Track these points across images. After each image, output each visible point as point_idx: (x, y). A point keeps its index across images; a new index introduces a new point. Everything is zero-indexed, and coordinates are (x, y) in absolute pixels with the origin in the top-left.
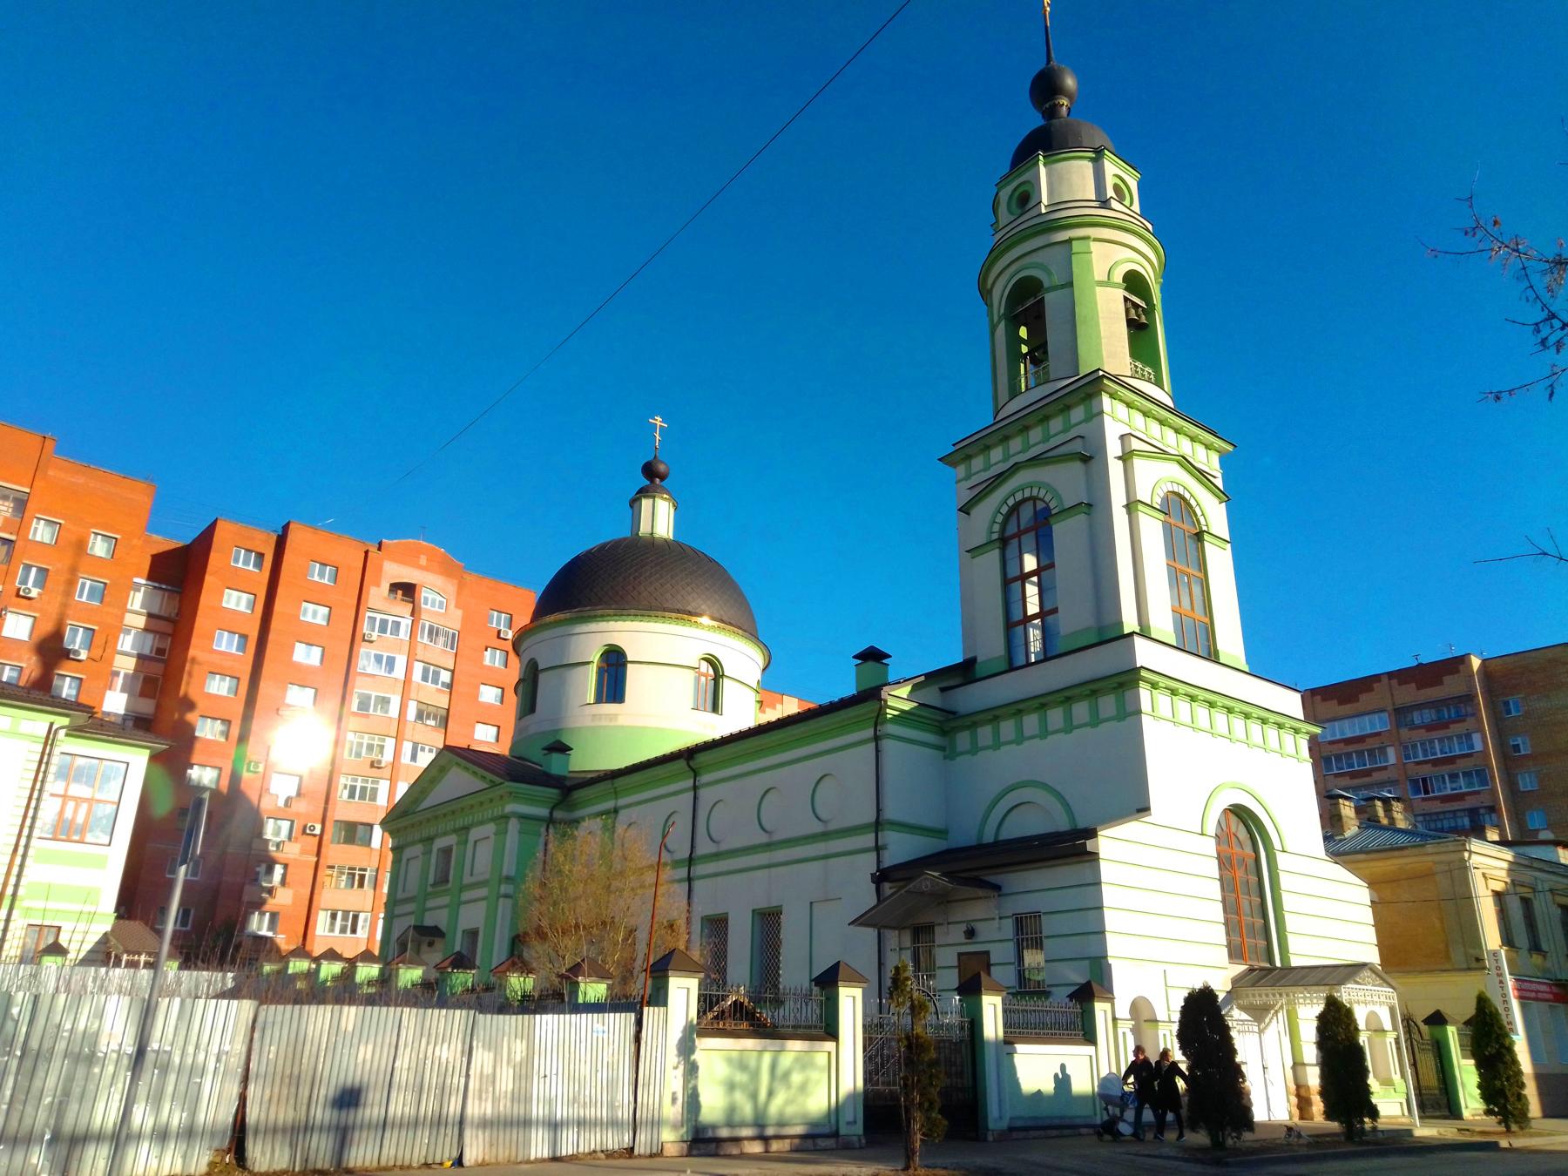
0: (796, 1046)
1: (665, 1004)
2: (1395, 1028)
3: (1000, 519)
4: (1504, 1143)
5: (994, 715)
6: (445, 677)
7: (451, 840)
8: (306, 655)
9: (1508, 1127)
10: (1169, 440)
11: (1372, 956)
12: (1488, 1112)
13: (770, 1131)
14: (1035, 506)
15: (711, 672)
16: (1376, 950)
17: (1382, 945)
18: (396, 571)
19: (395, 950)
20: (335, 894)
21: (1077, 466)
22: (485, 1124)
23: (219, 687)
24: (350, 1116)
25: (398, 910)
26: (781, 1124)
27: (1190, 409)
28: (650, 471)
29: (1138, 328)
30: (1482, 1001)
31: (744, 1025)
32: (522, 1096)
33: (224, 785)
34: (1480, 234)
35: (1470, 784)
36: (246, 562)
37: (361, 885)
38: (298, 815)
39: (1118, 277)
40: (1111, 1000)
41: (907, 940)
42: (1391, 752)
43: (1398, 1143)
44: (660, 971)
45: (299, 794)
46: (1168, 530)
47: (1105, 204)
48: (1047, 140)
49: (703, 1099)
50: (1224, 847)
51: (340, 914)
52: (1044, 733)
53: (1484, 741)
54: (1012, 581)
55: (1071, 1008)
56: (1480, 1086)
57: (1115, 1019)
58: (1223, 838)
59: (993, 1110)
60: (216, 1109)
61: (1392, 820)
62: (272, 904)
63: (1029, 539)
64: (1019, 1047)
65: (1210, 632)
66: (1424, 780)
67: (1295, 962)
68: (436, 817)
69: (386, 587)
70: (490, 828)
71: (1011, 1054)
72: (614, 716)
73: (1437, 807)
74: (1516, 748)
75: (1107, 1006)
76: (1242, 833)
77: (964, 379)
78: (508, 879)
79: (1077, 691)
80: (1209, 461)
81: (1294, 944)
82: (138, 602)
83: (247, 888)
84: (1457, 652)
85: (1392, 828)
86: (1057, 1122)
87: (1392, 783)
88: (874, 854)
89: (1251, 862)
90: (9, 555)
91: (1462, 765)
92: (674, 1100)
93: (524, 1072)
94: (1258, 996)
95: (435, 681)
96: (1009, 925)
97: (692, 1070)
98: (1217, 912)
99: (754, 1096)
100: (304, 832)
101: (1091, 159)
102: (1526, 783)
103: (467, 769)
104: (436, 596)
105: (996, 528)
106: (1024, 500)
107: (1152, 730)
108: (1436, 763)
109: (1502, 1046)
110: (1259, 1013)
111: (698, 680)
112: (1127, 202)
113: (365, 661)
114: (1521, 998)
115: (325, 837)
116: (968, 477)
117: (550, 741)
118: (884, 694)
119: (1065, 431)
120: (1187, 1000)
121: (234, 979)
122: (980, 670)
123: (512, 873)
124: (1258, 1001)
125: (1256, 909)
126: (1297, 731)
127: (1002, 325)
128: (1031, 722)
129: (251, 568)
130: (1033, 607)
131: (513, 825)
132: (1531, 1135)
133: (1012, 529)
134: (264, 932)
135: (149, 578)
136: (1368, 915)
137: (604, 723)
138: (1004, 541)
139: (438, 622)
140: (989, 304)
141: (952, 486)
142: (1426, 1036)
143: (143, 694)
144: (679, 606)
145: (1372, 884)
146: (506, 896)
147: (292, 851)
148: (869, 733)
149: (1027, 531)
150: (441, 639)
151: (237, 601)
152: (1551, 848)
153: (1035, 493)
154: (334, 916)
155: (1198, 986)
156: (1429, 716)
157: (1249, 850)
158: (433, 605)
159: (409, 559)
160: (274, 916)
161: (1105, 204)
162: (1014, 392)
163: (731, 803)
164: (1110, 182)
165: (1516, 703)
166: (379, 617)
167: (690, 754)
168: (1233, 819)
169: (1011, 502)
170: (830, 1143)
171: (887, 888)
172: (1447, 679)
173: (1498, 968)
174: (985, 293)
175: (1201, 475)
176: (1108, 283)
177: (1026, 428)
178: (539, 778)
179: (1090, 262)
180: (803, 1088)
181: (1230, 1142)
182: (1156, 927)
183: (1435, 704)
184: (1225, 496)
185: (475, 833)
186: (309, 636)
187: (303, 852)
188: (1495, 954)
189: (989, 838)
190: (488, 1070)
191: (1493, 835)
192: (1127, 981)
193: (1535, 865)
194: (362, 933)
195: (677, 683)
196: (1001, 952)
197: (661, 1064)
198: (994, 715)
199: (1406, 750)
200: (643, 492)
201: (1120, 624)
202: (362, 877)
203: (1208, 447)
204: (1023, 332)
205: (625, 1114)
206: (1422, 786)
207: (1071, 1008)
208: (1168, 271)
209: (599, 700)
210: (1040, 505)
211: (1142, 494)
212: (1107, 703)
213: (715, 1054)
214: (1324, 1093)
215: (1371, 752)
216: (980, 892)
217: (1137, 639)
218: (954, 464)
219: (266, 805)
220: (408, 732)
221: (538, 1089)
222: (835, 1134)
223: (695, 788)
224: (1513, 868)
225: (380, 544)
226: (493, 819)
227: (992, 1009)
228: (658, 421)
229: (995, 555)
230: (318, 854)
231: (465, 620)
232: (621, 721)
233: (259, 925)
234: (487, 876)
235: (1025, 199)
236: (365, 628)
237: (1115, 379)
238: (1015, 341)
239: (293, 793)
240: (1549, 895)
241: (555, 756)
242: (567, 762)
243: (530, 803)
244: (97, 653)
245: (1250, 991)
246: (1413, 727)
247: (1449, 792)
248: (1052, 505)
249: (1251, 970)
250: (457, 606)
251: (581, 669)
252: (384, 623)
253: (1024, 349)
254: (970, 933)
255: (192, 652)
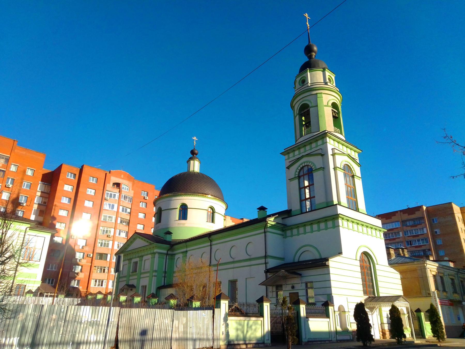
0: (253, 319)
1: (220, 307)
2: (408, 313)
3: (298, 171)
4: (439, 345)
5: (297, 226)
6: (129, 210)
7: (137, 259)
8: (88, 204)
9: (439, 341)
10: (345, 150)
11: (401, 293)
12: (434, 336)
13: (247, 342)
14: (308, 167)
15: (212, 211)
16: (402, 292)
17: (404, 290)
18: (114, 179)
19: (120, 291)
20: (96, 275)
21: (320, 157)
22: (177, 340)
23: (63, 213)
24: (144, 337)
25: (121, 280)
26: (250, 340)
27: (350, 140)
28: (193, 152)
29: (336, 118)
30: (432, 306)
31: (238, 313)
32: (185, 332)
33: (64, 242)
34: (447, 138)
35: (423, 243)
36: (71, 177)
37: (104, 272)
38: (86, 251)
39: (330, 104)
40: (333, 306)
41: (274, 289)
42: (401, 233)
43: (411, 344)
44: (218, 298)
45: (86, 245)
46: (345, 175)
47: (326, 84)
48: (309, 65)
49: (230, 333)
50: (362, 263)
51: (98, 281)
52: (312, 231)
53: (427, 230)
54: (302, 188)
55: (323, 308)
56: (431, 329)
57: (334, 311)
58: (361, 261)
59: (303, 337)
60: (111, 336)
61: (404, 254)
62: (78, 277)
63: (306, 177)
64: (310, 319)
65: (356, 203)
66: (410, 241)
67: (381, 295)
68: (130, 254)
69: (111, 184)
70: (150, 256)
71: (308, 321)
72: (184, 224)
73: (414, 249)
74: (436, 232)
75: (332, 307)
76: (366, 259)
77: (286, 132)
78: (156, 271)
79: (321, 220)
80: (355, 155)
81: (381, 290)
82: (39, 187)
83: (71, 273)
84: (419, 205)
85: (404, 256)
86: (320, 340)
87: (402, 242)
88: (265, 265)
89: (368, 267)
90: (4, 175)
91: (421, 237)
92: (223, 334)
93: (186, 326)
94: (371, 304)
95: (126, 212)
96: (304, 285)
97: (227, 325)
98: (360, 281)
99: (243, 332)
100: (87, 256)
101: (322, 71)
102: (439, 242)
103: (142, 239)
104: (126, 187)
105: (297, 173)
106: (305, 166)
107: (342, 231)
108: (414, 236)
109: (437, 318)
110: (372, 309)
111: (208, 213)
112: (332, 83)
113: (106, 206)
114: (441, 305)
115: (94, 258)
116: (289, 158)
117: (165, 231)
118: (267, 220)
119: (316, 147)
120: (356, 306)
121: (80, 300)
122: (293, 213)
123: (157, 269)
124: (372, 306)
125: (370, 281)
126: (380, 231)
127: (298, 116)
128: (308, 228)
129: (72, 178)
130: (308, 196)
131: (157, 255)
132: (445, 342)
133: (301, 174)
134: (75, 286)
135: (41, 181)
136: (400, 282)
137: (181, 226)
138: (299, 177)
139: (127, 194)
140: (294, 111)
141: (283, 161)
142: (416, 315)
143: (40, 215)
144: (203, 192)
145: (401, 272)
146: (155, 276)
147: (84, 262)
148: (263, 231)
149: (306, 174)
150: (128, 199)
151: (68, 188)
152: (448, 262)
153: (308, 164)
154: (96, 281)
155: (359, 302)
156: (411, 223)
157: (368, 264)
158: (125, 189)
159: (118, 176)
160: (78, 281)
161: (326, 84)
162: (301, 136)
163: (222, 249)
164: (327, 77)
165: (436, 220)
166: (109, 193)
167: (209, 235)
168: (364, 255)
169: (301, 166)
170: (262, 345)
171: (269, 275)
172: (416, 212)
173: (435, 296)
174: (292, 107)
175: (353, 159)
176: (327, 106)
177: (305, 146)
178: (162, 240)
179: (322, 100)
180: (255, 330)
181: (368, 344)
182: (345, 285)
183: (413, 220)
184: (360, 165)
185: (145, 258)
186: (90, 198)
187: (87, 262)
188: (434, 292)
189: (296, 260)
190: (177, 326)
191: (431, 259)
192: (337, 301)
193: (444, 267)
194: (104, 286)
195: (202, 215)
196: (302, 293)
197: (224, 324)
198: (297, 226)
199: (405, 233)
200: (191, 159)
201: (332, 201)
202: (104, 270)
203: (355, 151)
204: (303, 118)
205: (211, 337)
206: (410, 243)
207: (323, 308)
208: (343, 101)
209: (179, 219)
210: (309, 167)
211: (338, 165)
212: (330, 224)
213: (233, 321)
214: (391, 331)
215: (395, 233)
216: (296, 276)
217: (338, 206)
218: (284, 155)
219: (76, 248)
220: (118, 227)
221: (189, 330)
222: (264, 343)
223: (211, 245)
224: (438, 268)
225: (110, 171)
226: (151, 254)
227: (303, 309)
228: (195, 138)
229: (297, 181)
230: (92, 263)
231: (134, 194)
232: (186, 225)
233: (74, 284)
234: (149, 270)
235: (304, 81)
236: (105, 196)
237: (330, 133)
238: (301, 121)
239: (84, 245)
240: (448, 276)
241: (168, 235)
242: (171, 237)
243: (161, 249)
244: (28, 203)
245: (370, 303)
246: (407, 226)
247: (417, 245)
248: (313, 168)
249: (369, 297)
250: (132, 190)
251: (175, 210)
252: (111, 195)
253: (304, 123)
254: (293, 287)
255: (55, 203)
